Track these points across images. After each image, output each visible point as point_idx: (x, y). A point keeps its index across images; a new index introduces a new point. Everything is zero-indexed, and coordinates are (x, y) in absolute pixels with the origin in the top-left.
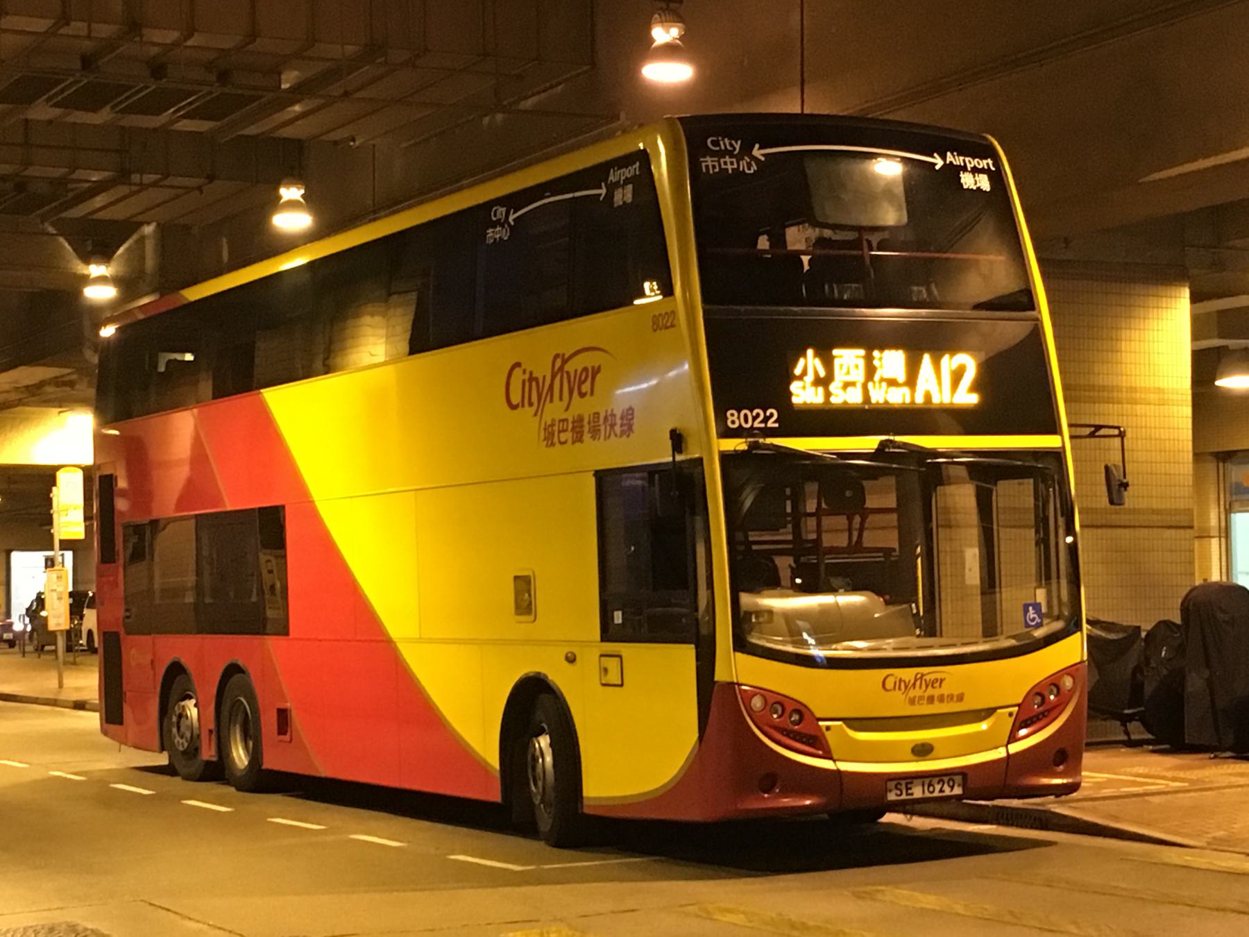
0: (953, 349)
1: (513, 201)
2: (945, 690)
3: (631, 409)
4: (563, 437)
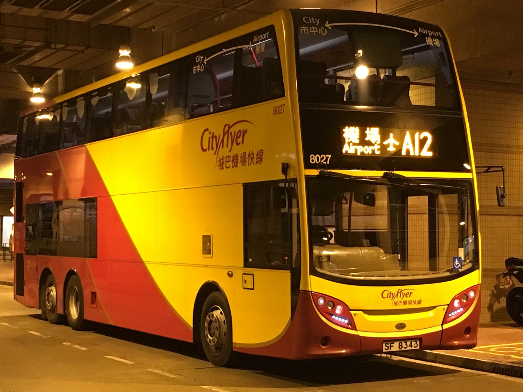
0: (421, 130)
1: (206, 53)
2: (412, 298)
3: (262, 150)
4: (228, 164)
